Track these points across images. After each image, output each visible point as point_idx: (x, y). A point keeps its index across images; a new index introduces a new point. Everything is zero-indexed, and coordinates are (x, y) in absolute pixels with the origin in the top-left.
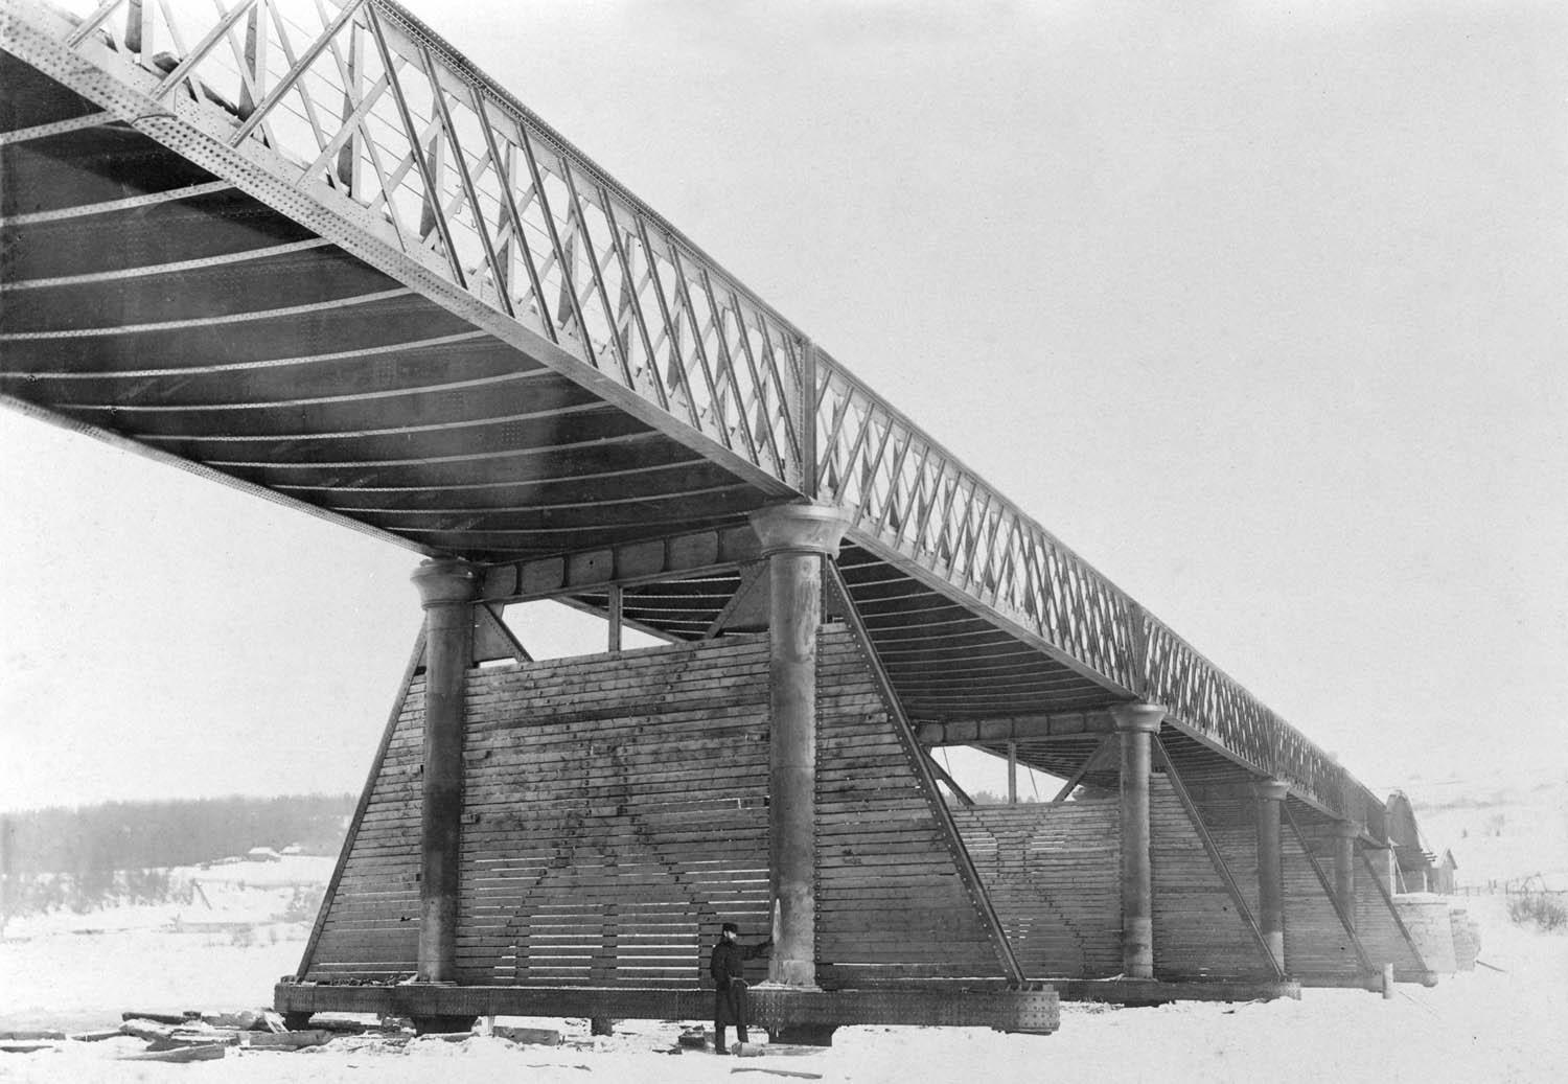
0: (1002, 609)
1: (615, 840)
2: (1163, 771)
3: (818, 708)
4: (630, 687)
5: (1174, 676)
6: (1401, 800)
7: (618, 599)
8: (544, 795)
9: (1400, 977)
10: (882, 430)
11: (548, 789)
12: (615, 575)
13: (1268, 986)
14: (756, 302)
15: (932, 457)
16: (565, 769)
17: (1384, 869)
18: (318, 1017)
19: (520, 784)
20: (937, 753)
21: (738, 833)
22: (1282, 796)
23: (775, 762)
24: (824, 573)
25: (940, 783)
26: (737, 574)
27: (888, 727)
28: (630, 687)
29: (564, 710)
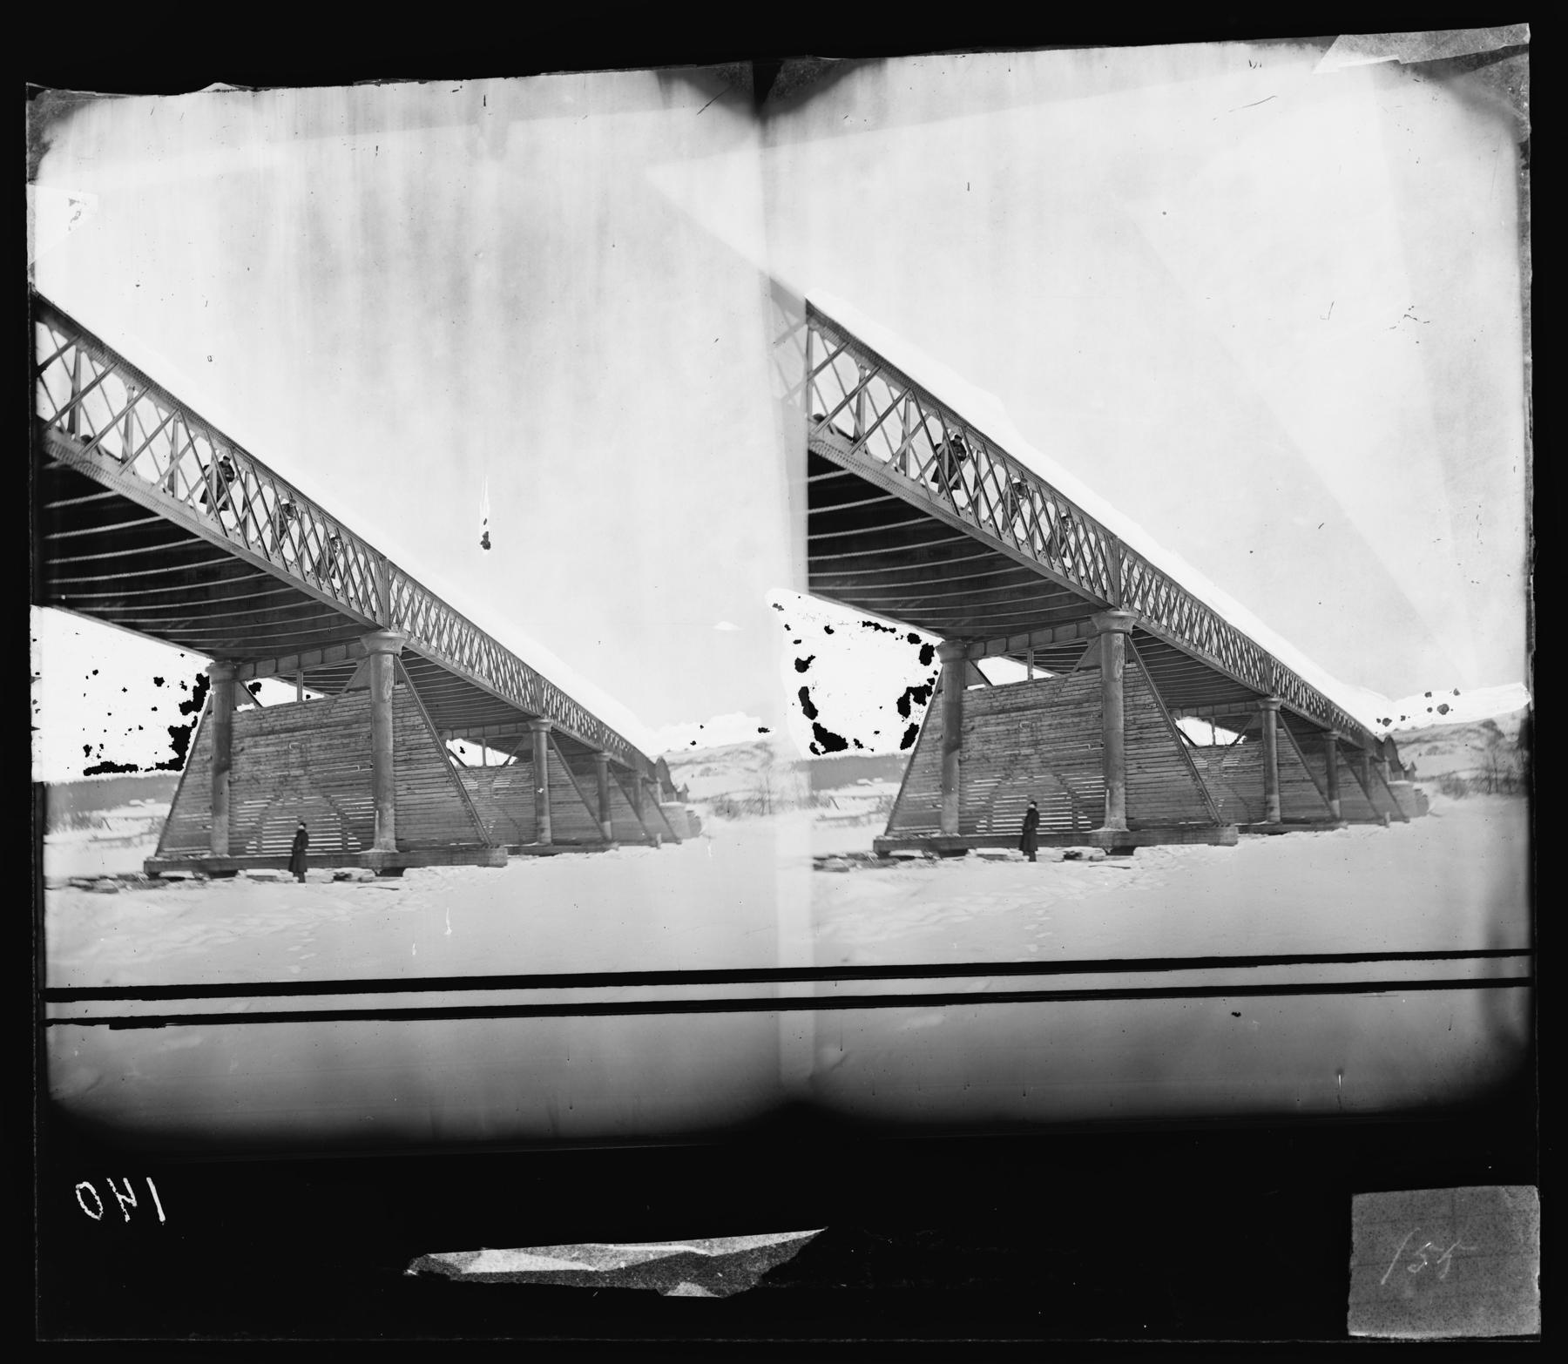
0: (477, 677)
1: (301, 787)
2: (552, 749)
3: (1124, 702)
4: (1038, 695)
5: (1285, 685)
6: (661, 761)
7: (1031, 655)
8: (268, 767)
9: (665, 841)
10: (1150, 577)
11: (270, 764)
12: (299, 666)
13: (1333, 824)
14: (361, 540)
15: (443, 610)
16: (1008, 734)
17: (1384, 770)
18: (893, 853)
19: (258, 763)
20: (1179, 724)
21: (358, 782)
22: (607, 759)
23: (374, 749)
24: (395, 662)
25: (451, 758)
26: (355, 664)
27: (426, 731)
28: (1038, 695)
29: (277, 728)
